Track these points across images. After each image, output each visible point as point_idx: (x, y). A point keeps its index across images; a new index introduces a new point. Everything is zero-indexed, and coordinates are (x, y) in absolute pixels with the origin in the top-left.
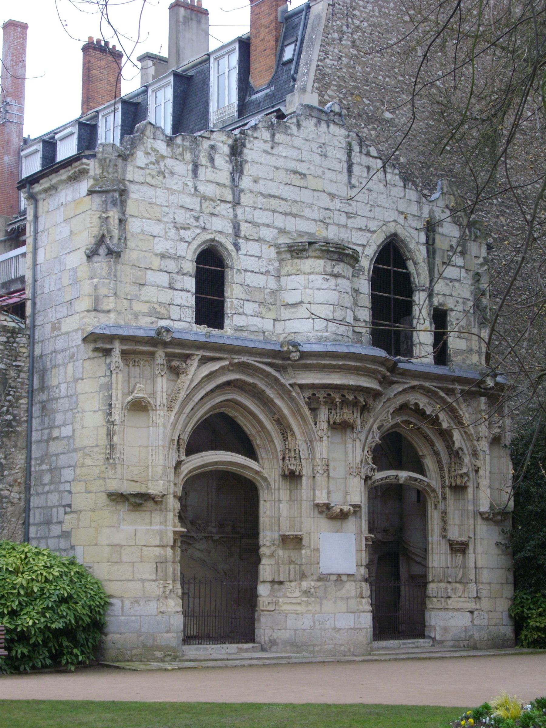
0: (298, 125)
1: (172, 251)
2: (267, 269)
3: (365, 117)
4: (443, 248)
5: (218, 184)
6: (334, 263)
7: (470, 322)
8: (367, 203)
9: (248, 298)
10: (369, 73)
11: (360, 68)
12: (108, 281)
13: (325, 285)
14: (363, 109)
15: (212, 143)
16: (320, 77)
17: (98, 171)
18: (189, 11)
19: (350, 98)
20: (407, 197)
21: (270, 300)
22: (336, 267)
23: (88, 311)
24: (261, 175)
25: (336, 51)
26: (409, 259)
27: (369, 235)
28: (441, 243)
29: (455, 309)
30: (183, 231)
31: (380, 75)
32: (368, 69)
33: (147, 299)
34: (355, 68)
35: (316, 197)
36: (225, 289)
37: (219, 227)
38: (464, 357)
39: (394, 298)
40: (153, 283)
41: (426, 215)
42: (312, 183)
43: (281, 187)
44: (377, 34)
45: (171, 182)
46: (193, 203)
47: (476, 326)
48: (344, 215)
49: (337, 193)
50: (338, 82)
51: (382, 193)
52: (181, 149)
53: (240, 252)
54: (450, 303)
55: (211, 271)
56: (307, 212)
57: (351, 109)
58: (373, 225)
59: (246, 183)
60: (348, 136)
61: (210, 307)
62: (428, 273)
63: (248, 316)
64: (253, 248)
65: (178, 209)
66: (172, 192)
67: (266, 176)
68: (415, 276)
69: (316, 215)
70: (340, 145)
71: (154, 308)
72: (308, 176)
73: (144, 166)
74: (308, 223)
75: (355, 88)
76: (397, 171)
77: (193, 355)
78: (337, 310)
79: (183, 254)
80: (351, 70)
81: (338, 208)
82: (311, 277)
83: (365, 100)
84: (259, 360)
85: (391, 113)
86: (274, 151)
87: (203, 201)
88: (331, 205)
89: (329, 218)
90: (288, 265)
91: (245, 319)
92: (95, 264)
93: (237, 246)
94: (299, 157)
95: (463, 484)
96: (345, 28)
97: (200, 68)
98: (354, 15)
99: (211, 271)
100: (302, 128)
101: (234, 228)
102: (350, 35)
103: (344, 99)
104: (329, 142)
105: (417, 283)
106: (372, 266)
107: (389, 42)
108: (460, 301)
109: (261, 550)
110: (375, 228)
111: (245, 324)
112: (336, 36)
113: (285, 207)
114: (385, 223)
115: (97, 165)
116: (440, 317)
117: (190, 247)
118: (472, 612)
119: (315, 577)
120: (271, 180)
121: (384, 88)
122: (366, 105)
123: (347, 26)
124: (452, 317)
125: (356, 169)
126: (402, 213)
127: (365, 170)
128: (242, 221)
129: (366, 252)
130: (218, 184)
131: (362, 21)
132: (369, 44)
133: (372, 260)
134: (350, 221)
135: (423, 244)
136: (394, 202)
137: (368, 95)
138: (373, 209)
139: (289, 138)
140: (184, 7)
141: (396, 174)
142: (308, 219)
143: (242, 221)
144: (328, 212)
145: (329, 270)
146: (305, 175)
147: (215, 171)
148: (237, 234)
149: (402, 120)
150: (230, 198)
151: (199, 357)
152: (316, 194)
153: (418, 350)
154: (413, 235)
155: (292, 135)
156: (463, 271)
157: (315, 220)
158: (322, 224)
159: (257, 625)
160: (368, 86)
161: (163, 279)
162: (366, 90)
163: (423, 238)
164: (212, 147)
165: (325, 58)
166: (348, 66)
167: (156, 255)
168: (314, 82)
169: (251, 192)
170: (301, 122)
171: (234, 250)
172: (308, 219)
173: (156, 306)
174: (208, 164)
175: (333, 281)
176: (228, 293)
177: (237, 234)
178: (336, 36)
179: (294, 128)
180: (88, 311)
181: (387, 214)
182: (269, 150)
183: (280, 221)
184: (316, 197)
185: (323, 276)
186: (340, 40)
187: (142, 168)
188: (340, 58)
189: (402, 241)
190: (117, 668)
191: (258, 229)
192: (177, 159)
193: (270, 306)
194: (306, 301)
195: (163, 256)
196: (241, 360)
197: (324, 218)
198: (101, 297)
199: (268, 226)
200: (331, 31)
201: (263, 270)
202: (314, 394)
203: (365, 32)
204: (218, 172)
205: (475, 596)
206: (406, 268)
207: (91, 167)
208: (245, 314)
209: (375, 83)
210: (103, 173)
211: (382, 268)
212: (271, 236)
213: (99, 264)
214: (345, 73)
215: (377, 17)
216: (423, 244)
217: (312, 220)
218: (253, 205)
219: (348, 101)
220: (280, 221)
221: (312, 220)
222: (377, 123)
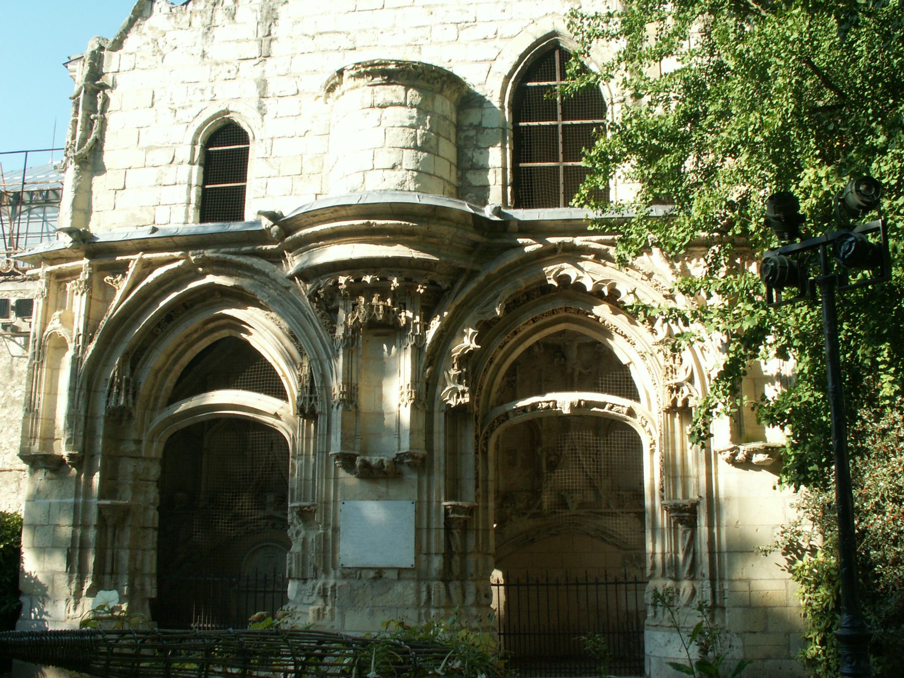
55: (223, 154)
77: (128, 262)
84: (232, 250)
99: (223, 154)
117: (191, 126)
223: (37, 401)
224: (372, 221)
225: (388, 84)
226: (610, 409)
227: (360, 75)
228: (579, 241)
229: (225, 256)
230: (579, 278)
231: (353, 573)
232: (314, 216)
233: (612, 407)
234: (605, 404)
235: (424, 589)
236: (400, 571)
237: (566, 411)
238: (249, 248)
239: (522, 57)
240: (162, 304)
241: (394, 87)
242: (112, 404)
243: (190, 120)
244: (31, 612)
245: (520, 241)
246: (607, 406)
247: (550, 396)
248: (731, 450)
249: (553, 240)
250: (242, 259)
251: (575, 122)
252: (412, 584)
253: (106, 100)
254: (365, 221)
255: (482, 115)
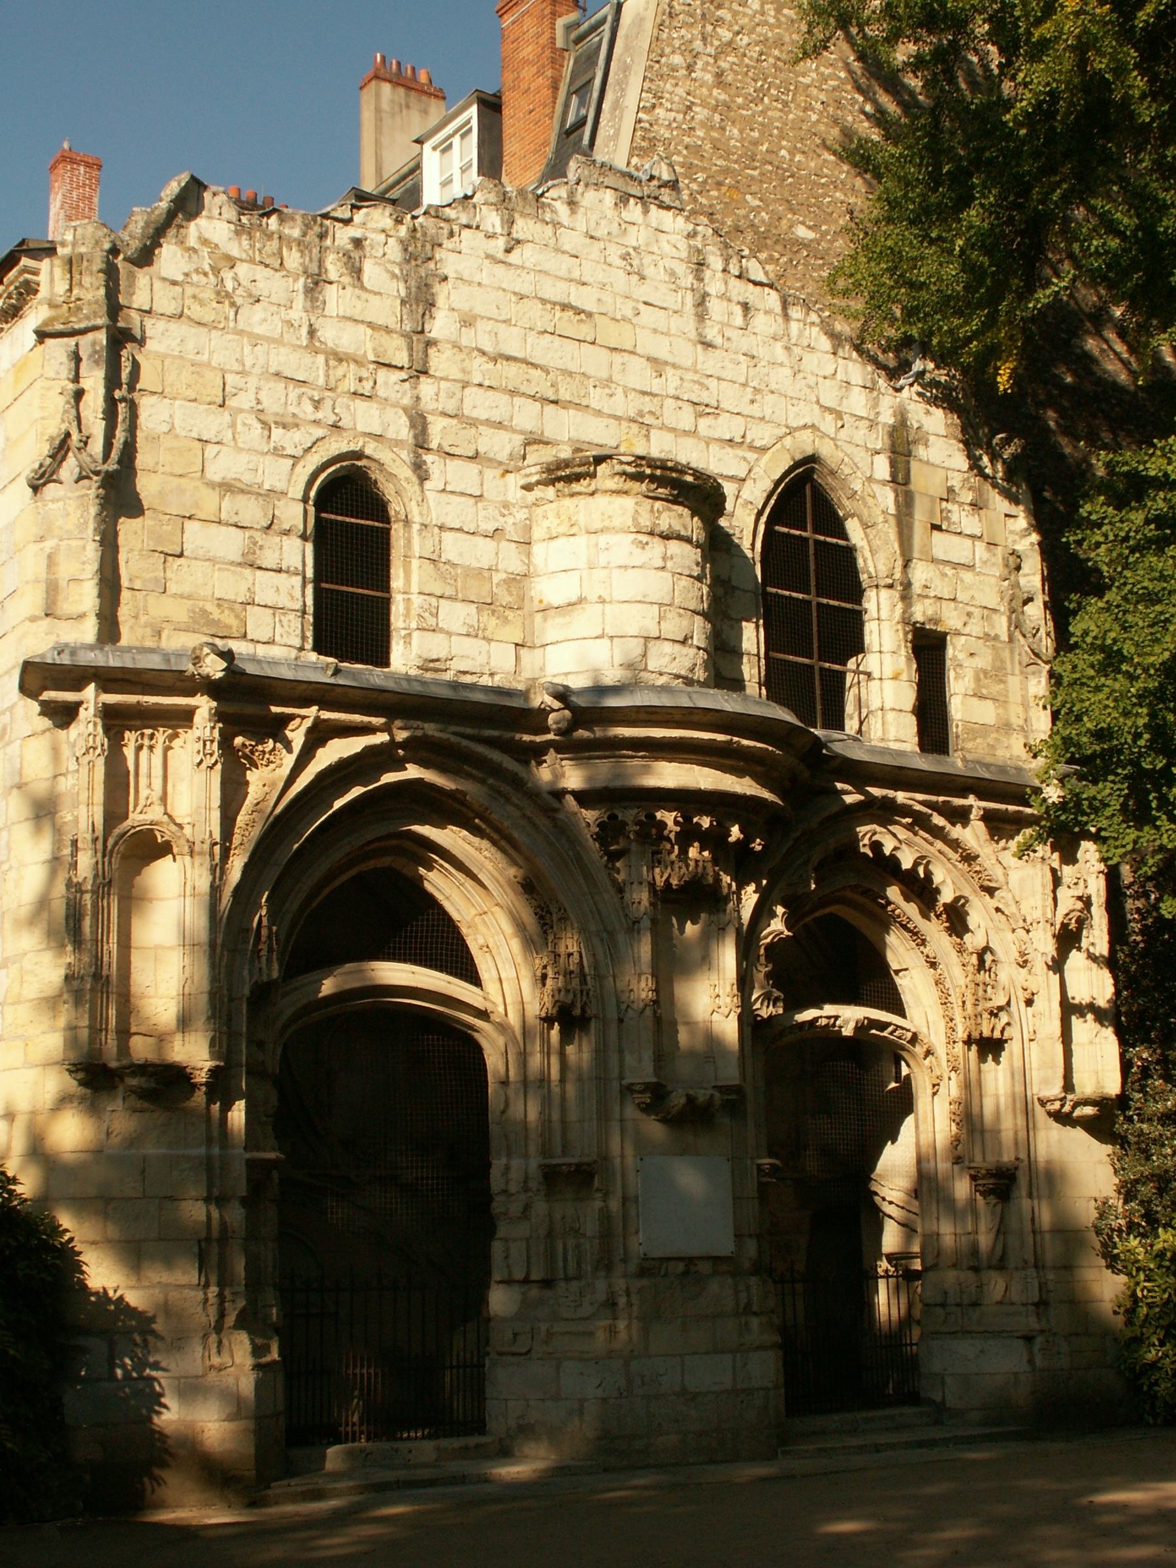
0: (572, 203)
1: (247, 478)
2: (496, 525)
3: (749, 236)
4: (931, 492)
5: (370, 325)
6: (658, 505)
7: (1002, 661)
8: (745, 385)
9: (449, 592)
10: (756, 143)
11: (736, 131)
12: (81, 543)
13: (640, 557)
14: (746, 217)
15: (357, 233)
16: (643, 144)
17: (61, 287)
18: (401, 91)
19: (714, 193)
20: (839, 376)
21: (506, 599)
22: (665, 515)
23: (33, 619)
24: (479, 310)
25: (680, 91)
26: (852, 516)
27: (752, 456)
28: (923, 481)
29: (967, 630)
30: (281, 431)
31: (784, 148)
32: (756, 134)
33: (186, 589)
34: (723, 129)
35: (617, 367)
36: (392, 571)
37: (374, 426)
38: (990, 741)
39: (819, 605)
40: (201, 552)
41: (887, 418)
42: (612, 334)
43: (529, 340)
44: (771, 60)
45: (254, 318)
46: (314, 368)
47: (1017, 671)
48: (688, 409)
49: (670, 359)
50: (685, 157)
51: (781, 365)
52: (275, 243)
53: (428, 485)
54: (951, 619)
55: (350, 526)
56: (596, 398)
57: (718, 216)
58: (762, 435)
59: (441, 326)
60: (692, 235)
61: (350, 608)
62: (896, 546)
63: (449, 634)
64: (462, 475)
65: (268, 380)
66: (256, 340)
67: (494, 313)
68: (868, 554)
69: (621, 405)
70: (675, 253)
71: (204, 612)
72: (596, 316)
73: (180, 278)
74: (601, 422)
75: (726, 171)
76: (813, 317)
77: (292, 717)
78: (669, 615)
79: (280, 486)
80: (715, 134)
81: (672, 392)
82: (603, 539)
83: (748, 197)
84: (469, 731)
85: (810, 228)
86: (514, 257)
87: (332, 363)
88: (656, 386)
89: (651, 412)
90: (550, 515)
91: (431, 637)
92: (51, 505)
93: (421, 471)
94: (576, 274)
95: (997, 1035)
96: (698, 44)
97: (409, 182)
98: (720, 20)
99: (350, 526)
100: (582, 210)
101: (413, 426)
102: (711, 60)
103: (700, 193)
104: (648, 245)
105: (872, 569)
106: (762, 528)
107: (801, 79)
108: (977, 612)
109: (494, 1205)
110: (764, 442)
111: (443, 655)
112: (677, 59)
113: (539, 383)
114: (791, 431)
115: (58, 272)
116: (928, 649)
117: (299, 468)
118: (1029, 1339)
119: (632, 1267)
120: (504, 321)
121: (792, 176)
122: (753, 209)
123: (704, 39)
124: (954, 651)
125: (715, 307)
126: (830, 410)
127: (738, 310)
128: (432, 413)
129: (745, 494)
130: (370, 325)
131: (738, 33)
132: (755, 81)
133: (760, 514)
134: (703, 423)
135: (884, 483)
136: (810, 387)
137: (754, 188)
138: (758, 397)
139: (549, 229)
140: (390, 81)
141: (813, 324)
142: (599, 413)
143: (432, 413)
144: (647, 398)
145: (646, 521)
146: (590, 315)
147: (365, 295)
148: (421, 444)
149: (837, 244)
150: (402, 358)
151: (308, 723)
152: (617, 358)
153: (879, 725)
154: (857, 460)
155: (556, 225)
156: (980, 547)
157: (618, 418)
158: (635, 426)
159: (489, 1391)
160: (754, 169)
161: (230, 543)
162: (752, 178)
163: (882, 468)
164: (358, 243)
165: (654, 106)
166: (707, 125)
167: (212, 485)
168: (631, 155)
169: (457, 346)
170: (578, 198)
171: (415, 479)
172: (599, 413)
173: (210, 607)
174: (346, 280)
175: (657, 545)
176: (397, 582)
177: (421, 444)
178: (677, 59)
179: (562, 209)
180: (33, 619)
181: (792, 411)
182: (500, 255)
183: (527, 416)
184: (617, 367)
185: (633, 536)
186: (690, 68)
187: (174, 283)
188: (689, 108)
189: (833, 473)
190: (1033, 1220)
191: (473, 430)
192: (267, 266)
193: (507, 612)
194: (593, 597)
195: (227, 488)
196: (419, 733)
197: (641, 414)
198: (63, 583)
199: (499, 425)
200: (667, 50)
201: (490, 527)
202: (613, 817)
203: (745, 55)
204: (370, 297)
205: (1036, 1299)
206: (845, 537)
207: (43, 278)
208: (442, 631)
209: (770, 163)
210: (70, 290)
211: (788, 535)
212: (507, 451)
213: (61, 504)
214: (703, 139)
215: (771, 27)
216: (884, 483)
217: (611, 416)
218: (459, 376)
219: (709, 198)
220: (527, 416)
221: (611, 416)
222: (779, 248)
223: (105, 959)
224: (736, 739)
225: (675, 502)
226: (891, 1033)
227: (638, 477)
228: (901, 797)
229: (459, 739)
230: (895, 849)
231: (649, 1268)
232: (652, 713)
233: (895, 1031)
234: (888, 1024)
235: (742, 1287)
236: (716, 1259)
237: (848, 1031)
238: (496, 733)
239: (777, 484)
240: (338, 804)
241: (680, 509)
242: (255, 977)
243: (298, 452)
244: (112, 1366)
245: (839, 786)
246: (891, 1028)
247: (829, 1009)
248: (1061, 1100)
249: (876, 792)
250: (480, 749)
251: (832, 602)
252: (730, 1281)
253: (136, 366)
254: (729, 737)
255: (732, 567)
